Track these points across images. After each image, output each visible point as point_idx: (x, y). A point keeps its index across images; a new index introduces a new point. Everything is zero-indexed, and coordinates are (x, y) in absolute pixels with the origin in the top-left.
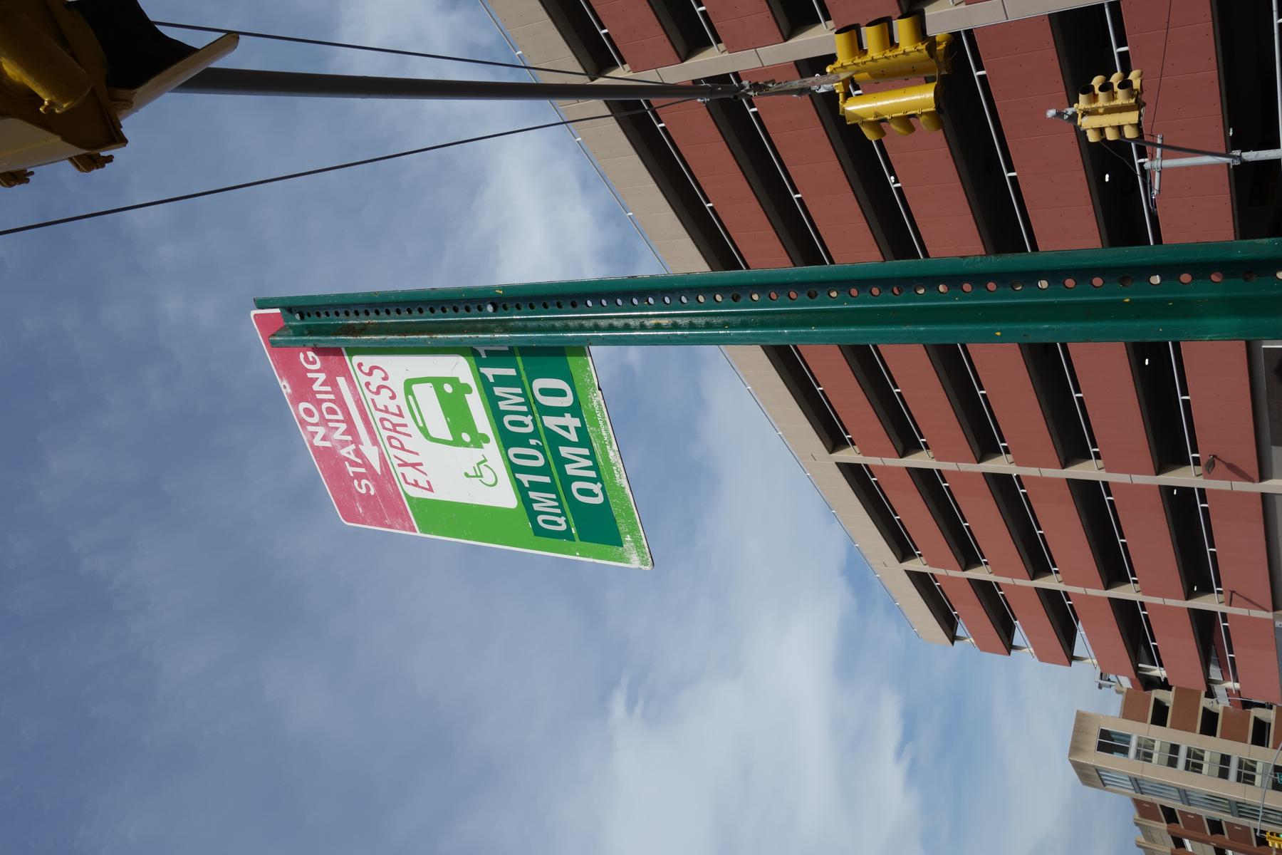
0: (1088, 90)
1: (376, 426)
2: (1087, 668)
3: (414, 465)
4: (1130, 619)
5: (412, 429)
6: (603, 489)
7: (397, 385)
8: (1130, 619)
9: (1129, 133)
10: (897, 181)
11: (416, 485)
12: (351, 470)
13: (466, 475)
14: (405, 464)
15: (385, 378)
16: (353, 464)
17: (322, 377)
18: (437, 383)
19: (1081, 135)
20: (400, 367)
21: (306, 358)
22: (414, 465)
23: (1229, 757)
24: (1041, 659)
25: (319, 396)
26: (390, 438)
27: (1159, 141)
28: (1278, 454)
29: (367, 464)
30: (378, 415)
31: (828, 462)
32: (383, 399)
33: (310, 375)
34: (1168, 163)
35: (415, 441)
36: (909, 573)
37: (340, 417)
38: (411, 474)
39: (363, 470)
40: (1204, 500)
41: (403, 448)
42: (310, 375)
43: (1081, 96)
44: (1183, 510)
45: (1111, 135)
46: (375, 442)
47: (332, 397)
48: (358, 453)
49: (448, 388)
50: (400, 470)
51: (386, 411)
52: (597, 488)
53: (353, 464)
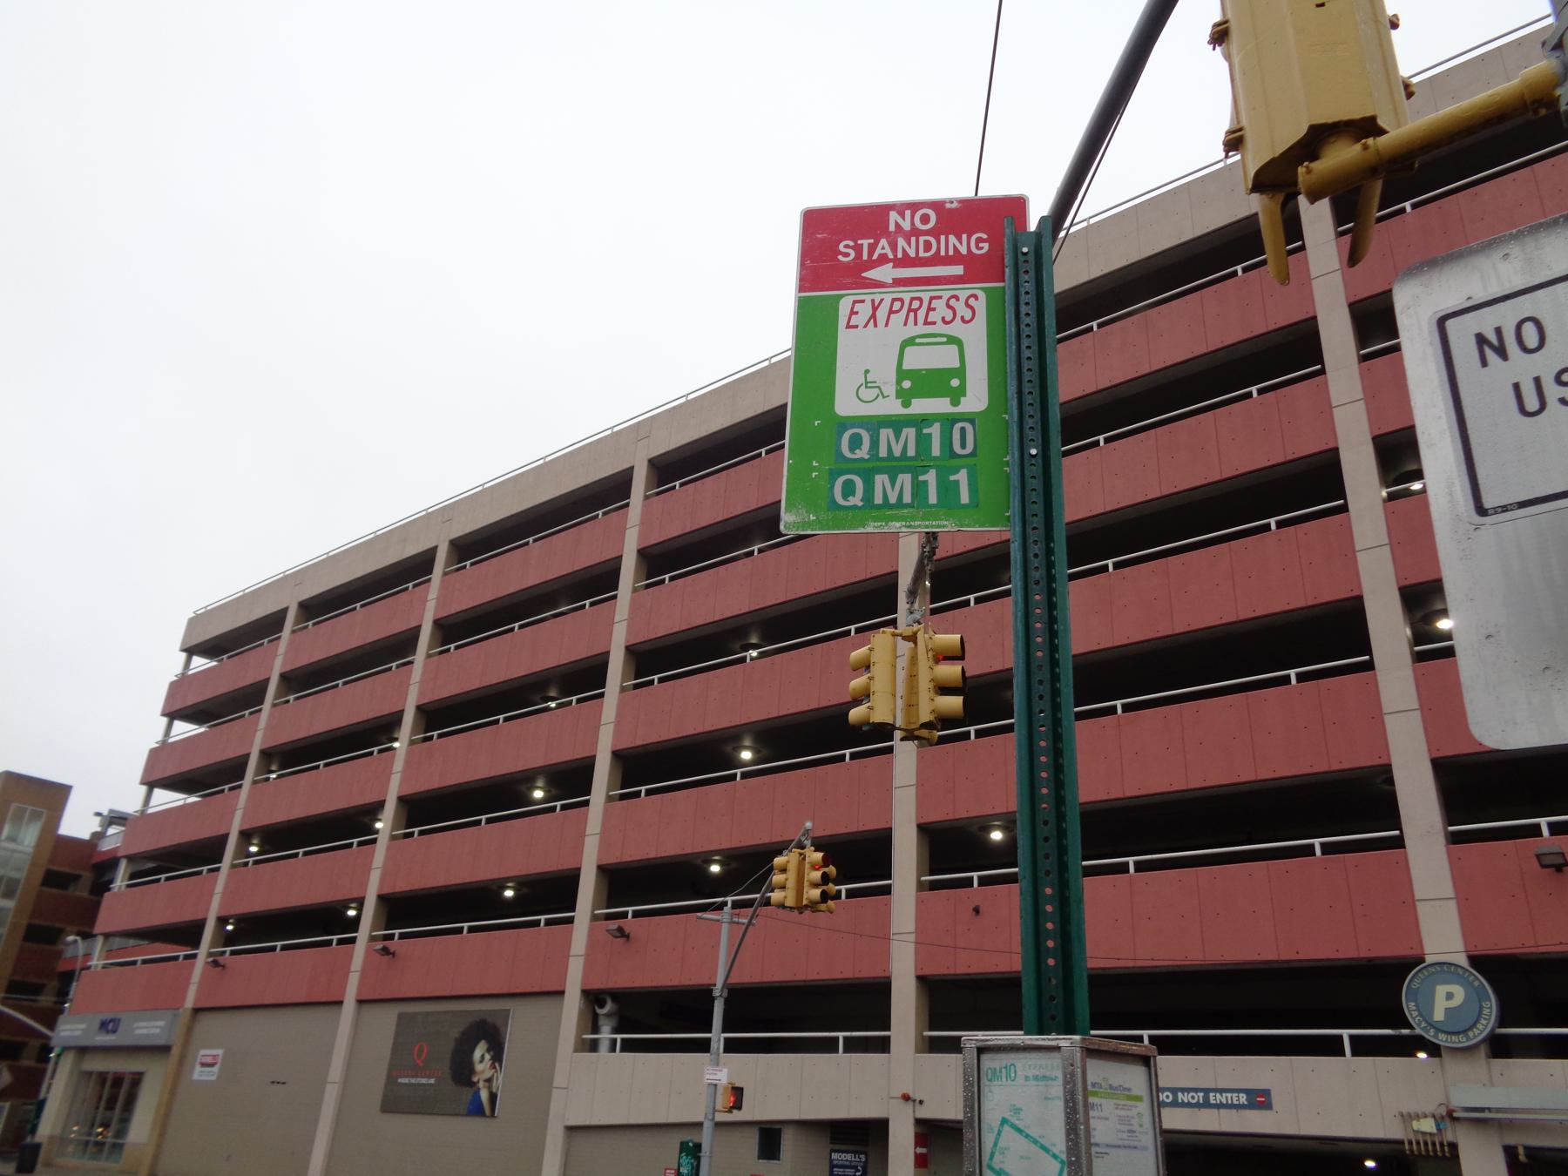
0: (826, 862)
1: (915, 291)
2: (130, 799)
3: (874, 316)
4: (206, 852)
5: (912, 330)
6: (855, 507)
7: (957, 329)
9: (776, 896)
10: (752, 659)
11: (853, 313)
12: (865, 243)
13: (867, 372)
14: (875, 309)
16: (872, 248)
17: (963, 250)
18: (960, 372)
19: (779, 849)
20: (976, 336)
21: (979, 240)
22: (874, 316)
24: (153, 752)
25: (943, 238)
26: (901, 300)
28: (385, 1021)
29: (872, 264)
30: (926, 297)
31: (291, 601)
32: (941, 310)
33: (964, 237)
34: (725, 929)
35: (899, 329)
36: (284, 611)
37: (922, 254)
38: (865, 310)
39: (865, 257)
41: (891, 312)
42: (964, 237)
43: (820, 855)
44: (326, 921)
45: (777, 878)
46: (898, 282)
47: (943, 253)
48: (883, 259)
49: (955, 383)
50: (868, 298)
51: (930, 309)
52: (856, 500)
53: (872, 248)
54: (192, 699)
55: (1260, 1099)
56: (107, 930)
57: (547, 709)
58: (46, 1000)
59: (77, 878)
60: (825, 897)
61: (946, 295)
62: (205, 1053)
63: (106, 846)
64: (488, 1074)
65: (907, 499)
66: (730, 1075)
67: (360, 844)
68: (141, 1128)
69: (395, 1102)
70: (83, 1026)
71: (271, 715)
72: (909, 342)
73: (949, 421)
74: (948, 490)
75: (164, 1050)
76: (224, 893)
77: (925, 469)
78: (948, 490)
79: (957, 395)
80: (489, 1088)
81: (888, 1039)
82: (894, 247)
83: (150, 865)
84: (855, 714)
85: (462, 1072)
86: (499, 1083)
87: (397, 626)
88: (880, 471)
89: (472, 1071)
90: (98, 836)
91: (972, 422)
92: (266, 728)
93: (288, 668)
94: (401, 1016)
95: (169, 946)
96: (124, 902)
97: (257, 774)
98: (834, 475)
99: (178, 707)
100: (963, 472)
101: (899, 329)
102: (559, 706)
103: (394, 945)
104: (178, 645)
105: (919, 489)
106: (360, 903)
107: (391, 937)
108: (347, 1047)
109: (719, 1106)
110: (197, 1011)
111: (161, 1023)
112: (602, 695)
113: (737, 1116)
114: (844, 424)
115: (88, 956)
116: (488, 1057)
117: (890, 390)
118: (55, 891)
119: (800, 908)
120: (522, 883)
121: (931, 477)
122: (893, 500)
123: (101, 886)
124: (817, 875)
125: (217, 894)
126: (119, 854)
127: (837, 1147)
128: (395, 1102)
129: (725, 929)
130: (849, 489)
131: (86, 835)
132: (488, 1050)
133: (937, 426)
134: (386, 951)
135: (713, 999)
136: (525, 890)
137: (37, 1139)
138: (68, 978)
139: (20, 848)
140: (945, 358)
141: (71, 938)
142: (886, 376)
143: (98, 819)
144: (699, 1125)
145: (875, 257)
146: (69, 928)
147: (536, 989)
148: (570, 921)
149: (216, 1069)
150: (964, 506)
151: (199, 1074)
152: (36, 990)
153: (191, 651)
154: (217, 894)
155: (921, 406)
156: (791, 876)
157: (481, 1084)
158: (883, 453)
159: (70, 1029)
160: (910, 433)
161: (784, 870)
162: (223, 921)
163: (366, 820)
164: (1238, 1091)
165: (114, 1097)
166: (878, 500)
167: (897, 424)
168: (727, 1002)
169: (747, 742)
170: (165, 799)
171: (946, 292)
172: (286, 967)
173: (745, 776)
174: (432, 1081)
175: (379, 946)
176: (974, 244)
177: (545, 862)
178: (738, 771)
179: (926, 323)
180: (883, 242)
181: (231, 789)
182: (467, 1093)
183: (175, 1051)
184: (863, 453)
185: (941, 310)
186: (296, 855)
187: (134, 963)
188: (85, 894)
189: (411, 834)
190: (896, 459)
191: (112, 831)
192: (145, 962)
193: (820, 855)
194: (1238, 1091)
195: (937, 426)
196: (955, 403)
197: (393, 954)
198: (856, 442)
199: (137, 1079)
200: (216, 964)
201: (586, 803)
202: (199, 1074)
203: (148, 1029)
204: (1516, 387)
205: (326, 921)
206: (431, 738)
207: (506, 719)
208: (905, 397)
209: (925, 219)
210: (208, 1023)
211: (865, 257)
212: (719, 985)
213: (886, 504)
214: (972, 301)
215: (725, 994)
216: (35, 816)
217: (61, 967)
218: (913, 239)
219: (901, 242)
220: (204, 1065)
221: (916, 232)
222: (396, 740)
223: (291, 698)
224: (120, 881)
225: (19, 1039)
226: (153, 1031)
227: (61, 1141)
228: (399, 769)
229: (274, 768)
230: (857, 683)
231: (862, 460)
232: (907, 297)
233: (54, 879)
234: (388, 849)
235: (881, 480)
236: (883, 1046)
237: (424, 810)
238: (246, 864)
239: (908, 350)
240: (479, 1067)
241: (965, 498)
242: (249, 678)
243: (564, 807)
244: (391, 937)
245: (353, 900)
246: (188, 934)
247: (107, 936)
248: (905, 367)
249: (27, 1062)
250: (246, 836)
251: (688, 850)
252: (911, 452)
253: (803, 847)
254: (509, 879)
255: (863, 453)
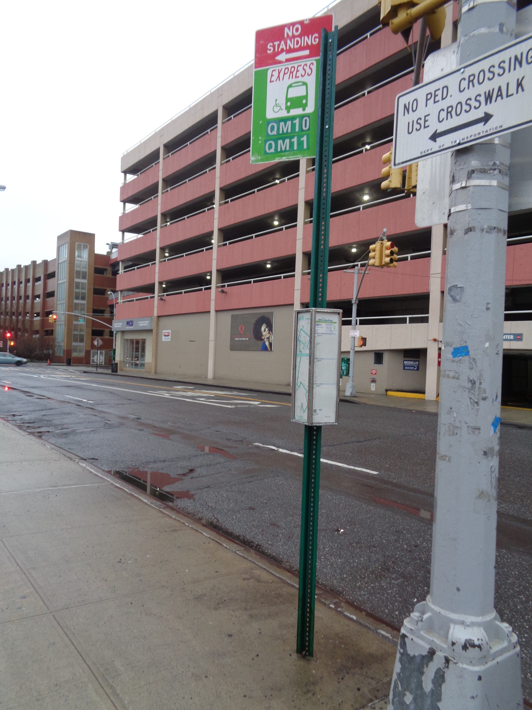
0: (392, 246)
2: (117, 238)
3: (279, 76)
6: (272, 153)
7: (306, 79)
8: (147, 258)
9: (371, 262)
10: (366, 150)
11: (272, 75)
12: (276, 43)
13: (276, 100)
14: (279, 73)
15: (308, 74)
16: (279, 46)
17: (310, 43)
18: (306, 97)
19: (373, 242)
21: (315, 38)
22: (279, 76)
23: (521, 339)
27: (366, 272)
28: (227, 318)
29: (279, 53)
32: (301, 72)
33: (310, 36)
34: (356, 276)
36: (158, 150)
37: (296, 46)
38: (276, 74)
39: (276, 50)
40: (206, 289)
41: (284, 74)
42: (310, 36)
43: (389, 243)
44: (199, 281)
45: (371, 254)
46: (288, 60)
47: (302, 45)
48: (282, 50)
52: (272, 150)
53: (279, 46)
54: (131, 193)
55: (518, 337)
56: (121, 289)
57: (276, 184)
58: (107, 315)
59: (106, 270)
60: (392, 261)
61: (303, 64)
62: (165, 331)
63: (114, 256)
64: (268, 336)
65: (288, 149)
66: (360, 333)
67: (206, 250)
68: (149, 357)
69: (234, 347)
70: (121, 324)
71: (162, 198)
72: (290, 86)
73: (302, 117)
74: (300, 144)
75: (151, 331)
76: (159, 273)
77: (293, 137)
78: (300, 144)
79: (304, 107)
80: (269, 341)
81: (428, 317)
82: (286, 44)
83: (130, 263)
84: (384, 184)
85: (258, 336)
86: (272, 339)
87: (206, 152)
88: (279, 139)
89: (262, 335)
90: (109, 253)
91: (309, 116)
92: (161, 203)
93: (165, 176)
94: (233, 316)
95: (145, 294)
96: (125, 279)
97: (161, 224)
98: (266, 141)
99: (125, 197)
100: (305, 137)
101: (287, 81)
102: (281, 182)
103: (226, 289)
104: (120, 171)
105: (291, 144)
106: (211, 272)
107: (224, 286)
108: (214, 328)
109: (356, 345)
110: (159, 317)
111: (148, 322)
112: (298, 176)
113: (364, 348)
114: (269, 122)
115: (117, 299)
116: (267, 330)
117: (284, 107)
118: (99, 275)
119: (382, 266)
120: (273, 261)
121: (295, 140)
122: (283, 149)
123: (115, 273)
124: (388, 252)
125: (157, 273)
126: (118, 260)
127: (406, 359)
128: (234, 347)
129: (356, 276)
130: (270, 147)
131: (105, 253)
132: (267, 327)
133: (298, 119)
134: (223, 292)
135: (352, 305)
136: (275, 264)
137: (116, 362)
138: (112, 307)
139: (83, 260)
140: (299, 92)
141: (109, 293)
142: (282, 101)
143: (108, 246)
144: (349, 352)
145: (280, 50)
146: (108, 289)
147: (283, 303)
148: (293, 276)
149: (170, 337)
150: (305, 150)
151: (164, 339)
152: (102, 312)
153: (126, 172)
154: (157, 273)
155: (294, 112)
156: (377, 253)
157: (265, 340)
158: (281, 132)
159: (117, 325)
160: (289, 123)
161: (374, 251)
162: (161, 283)
163: (208, 239)
164: (511, 334)
165: (137, 348)
166: (279, 150)
167: (284, 120)
168: (358, 305)
169: (367, 191)
170: (130, 237)
171: (302, 62)
172: (187, 299)
173: (364, 208)
174: (247, 339)
175: (220, 290)
176: (313, 40)
177: (282, 252)
178: (361, 206)
179: (296, 77)
180: (283, 42)
181: (153, 231)
182: (261, 343)
183: (154, 331)
184: (275, 133)
185: (301, 72)
186: (183, 256)
187: (133, 300)
188: (110, 276)
189: (226, 244)
190: (285, 134)
191: (114, 250)
192: (136, 300)
193: (389, 243)
194: (511, 334)
195: (298, 119)
196: (304, 110)
197: (226, 293)
198: (272, 128)
199: (144, 341)
200: (162, 299)
201: (296, 226)
202: (164, 339)
203: (144, 324)
204: (409, 123)
205: (199, 281)
206: (228, 202)
207: (258, 191)
208: (288, 109)
209: (297, 30)
210: (163, 321)
211: (276, 50)
212: (354, 299)
213: (281, 151)
214: (311, 66)
215: (357, 302)
216: (85, 247)
217: (109, 303)
218: (293, 40)
219: (289, 42)
220: (165, 336)
221: (294, 37)
222: (214, 204)
223: (169, 189)
224: (121, 271)
225: (102, 329)
226: (145, 325)
227: (124, 362)
228: (216, 218)
229: (168, 220)
230: (385, 170)
231: (274, 135)
232: (290, 67)
233: (98, 271)
234: (218, 251)
235: (280, 142)
236: (425, 320)
237: (231, 234)
238: (165, 261)
239: (290, 89)
240: (264, 333)
241: (305, 147)
242: (150, 182)
243: (286, 228)
244: (224, 286)
245: (208, 272)
246: (149, 289)
247: (121, 291)
248: (289, 97)
249: (107, 336)
250: (163, 249)
251: (340, 243)
252: (289, 131)
253: (382, 240)
254: (354, 243)
255: (275, 133)
